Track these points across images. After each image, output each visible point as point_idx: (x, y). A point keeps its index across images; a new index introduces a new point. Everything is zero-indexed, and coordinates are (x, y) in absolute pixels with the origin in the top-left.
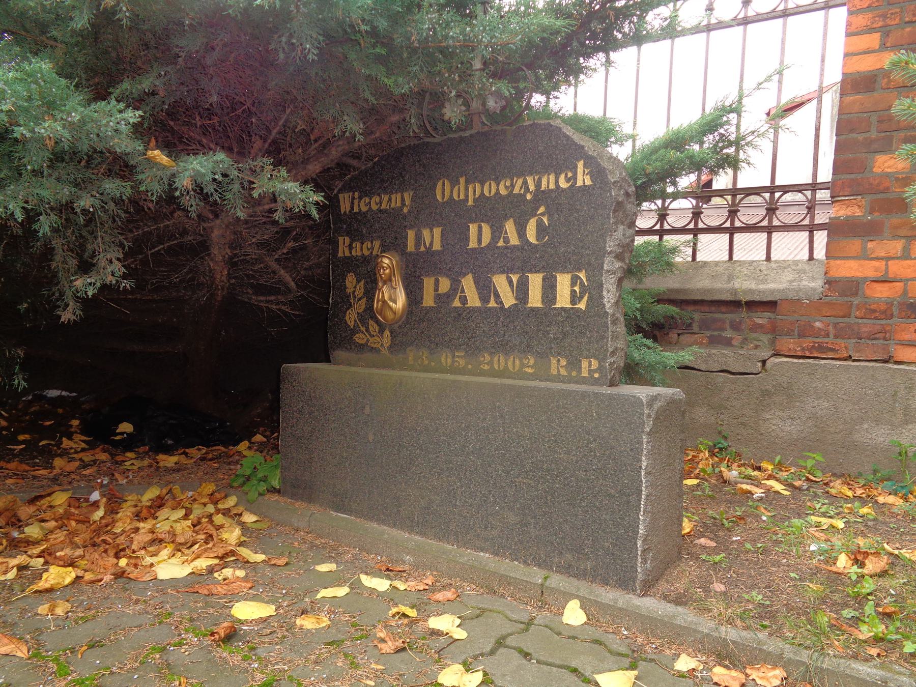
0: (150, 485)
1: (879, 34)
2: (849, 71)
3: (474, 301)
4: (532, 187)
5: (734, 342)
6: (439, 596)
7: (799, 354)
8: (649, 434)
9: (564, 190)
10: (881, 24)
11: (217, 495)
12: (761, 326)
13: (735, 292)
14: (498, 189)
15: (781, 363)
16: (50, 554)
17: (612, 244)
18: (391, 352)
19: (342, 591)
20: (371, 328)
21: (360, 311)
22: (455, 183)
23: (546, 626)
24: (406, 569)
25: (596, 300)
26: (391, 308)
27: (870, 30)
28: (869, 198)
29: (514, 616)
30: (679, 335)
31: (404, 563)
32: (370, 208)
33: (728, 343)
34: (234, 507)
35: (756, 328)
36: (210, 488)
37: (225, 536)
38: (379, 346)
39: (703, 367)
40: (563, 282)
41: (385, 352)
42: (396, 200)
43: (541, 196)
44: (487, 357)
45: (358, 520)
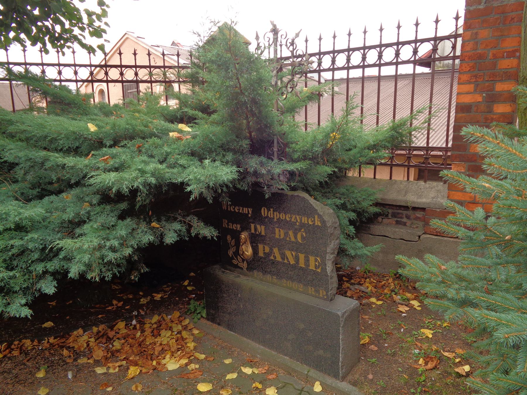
0: (154, 314)
1: (473, 85)
2: (459, 102)
3: (279, 259)
4: (299, 221)
5: (407, 224)
6: (270, 377)
7: (435, 234)
8: (342, 327)
9: (311, 225)
10: (474, 80)
11: (181, 319)
12: (419, 218)
13: (406, 202)
14: (286, 217)
15: (427, 238)
16: (128, 359)
17: (329, 250)
18: (247, 270)
19: (234, 376)
20: (239, 259)
21: (234, 251)
22: (269, 210)
23: (307, 392)
24: (258, 360)
25: (324, 270)
26: (246, 254)
27: (469, 82)
28: (468, 164)
29: (297, 387)
30: (382, 219)
31: (257, 357)
32: (235, 210)
33: (405, 224)
34: (188, 324)
35: (417, 218)
36: (177, 314)
37: (188, 345)
38: (242, 267)
39: (392, 237)
40: (312, 259)
41: (245, 269)
42: (245, 210)
43: (302, 225)
44: (285, 281)
45: (238, 336)
